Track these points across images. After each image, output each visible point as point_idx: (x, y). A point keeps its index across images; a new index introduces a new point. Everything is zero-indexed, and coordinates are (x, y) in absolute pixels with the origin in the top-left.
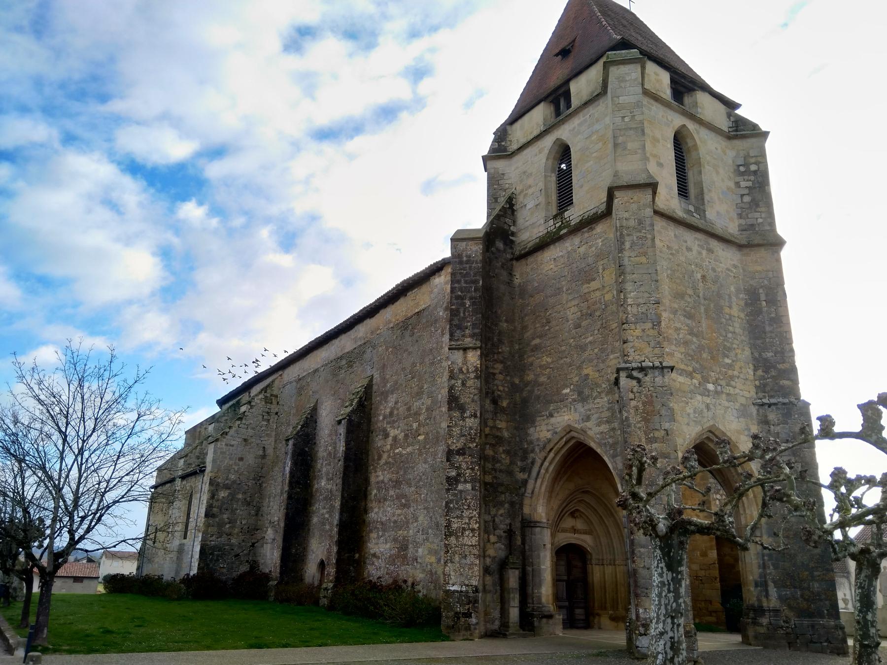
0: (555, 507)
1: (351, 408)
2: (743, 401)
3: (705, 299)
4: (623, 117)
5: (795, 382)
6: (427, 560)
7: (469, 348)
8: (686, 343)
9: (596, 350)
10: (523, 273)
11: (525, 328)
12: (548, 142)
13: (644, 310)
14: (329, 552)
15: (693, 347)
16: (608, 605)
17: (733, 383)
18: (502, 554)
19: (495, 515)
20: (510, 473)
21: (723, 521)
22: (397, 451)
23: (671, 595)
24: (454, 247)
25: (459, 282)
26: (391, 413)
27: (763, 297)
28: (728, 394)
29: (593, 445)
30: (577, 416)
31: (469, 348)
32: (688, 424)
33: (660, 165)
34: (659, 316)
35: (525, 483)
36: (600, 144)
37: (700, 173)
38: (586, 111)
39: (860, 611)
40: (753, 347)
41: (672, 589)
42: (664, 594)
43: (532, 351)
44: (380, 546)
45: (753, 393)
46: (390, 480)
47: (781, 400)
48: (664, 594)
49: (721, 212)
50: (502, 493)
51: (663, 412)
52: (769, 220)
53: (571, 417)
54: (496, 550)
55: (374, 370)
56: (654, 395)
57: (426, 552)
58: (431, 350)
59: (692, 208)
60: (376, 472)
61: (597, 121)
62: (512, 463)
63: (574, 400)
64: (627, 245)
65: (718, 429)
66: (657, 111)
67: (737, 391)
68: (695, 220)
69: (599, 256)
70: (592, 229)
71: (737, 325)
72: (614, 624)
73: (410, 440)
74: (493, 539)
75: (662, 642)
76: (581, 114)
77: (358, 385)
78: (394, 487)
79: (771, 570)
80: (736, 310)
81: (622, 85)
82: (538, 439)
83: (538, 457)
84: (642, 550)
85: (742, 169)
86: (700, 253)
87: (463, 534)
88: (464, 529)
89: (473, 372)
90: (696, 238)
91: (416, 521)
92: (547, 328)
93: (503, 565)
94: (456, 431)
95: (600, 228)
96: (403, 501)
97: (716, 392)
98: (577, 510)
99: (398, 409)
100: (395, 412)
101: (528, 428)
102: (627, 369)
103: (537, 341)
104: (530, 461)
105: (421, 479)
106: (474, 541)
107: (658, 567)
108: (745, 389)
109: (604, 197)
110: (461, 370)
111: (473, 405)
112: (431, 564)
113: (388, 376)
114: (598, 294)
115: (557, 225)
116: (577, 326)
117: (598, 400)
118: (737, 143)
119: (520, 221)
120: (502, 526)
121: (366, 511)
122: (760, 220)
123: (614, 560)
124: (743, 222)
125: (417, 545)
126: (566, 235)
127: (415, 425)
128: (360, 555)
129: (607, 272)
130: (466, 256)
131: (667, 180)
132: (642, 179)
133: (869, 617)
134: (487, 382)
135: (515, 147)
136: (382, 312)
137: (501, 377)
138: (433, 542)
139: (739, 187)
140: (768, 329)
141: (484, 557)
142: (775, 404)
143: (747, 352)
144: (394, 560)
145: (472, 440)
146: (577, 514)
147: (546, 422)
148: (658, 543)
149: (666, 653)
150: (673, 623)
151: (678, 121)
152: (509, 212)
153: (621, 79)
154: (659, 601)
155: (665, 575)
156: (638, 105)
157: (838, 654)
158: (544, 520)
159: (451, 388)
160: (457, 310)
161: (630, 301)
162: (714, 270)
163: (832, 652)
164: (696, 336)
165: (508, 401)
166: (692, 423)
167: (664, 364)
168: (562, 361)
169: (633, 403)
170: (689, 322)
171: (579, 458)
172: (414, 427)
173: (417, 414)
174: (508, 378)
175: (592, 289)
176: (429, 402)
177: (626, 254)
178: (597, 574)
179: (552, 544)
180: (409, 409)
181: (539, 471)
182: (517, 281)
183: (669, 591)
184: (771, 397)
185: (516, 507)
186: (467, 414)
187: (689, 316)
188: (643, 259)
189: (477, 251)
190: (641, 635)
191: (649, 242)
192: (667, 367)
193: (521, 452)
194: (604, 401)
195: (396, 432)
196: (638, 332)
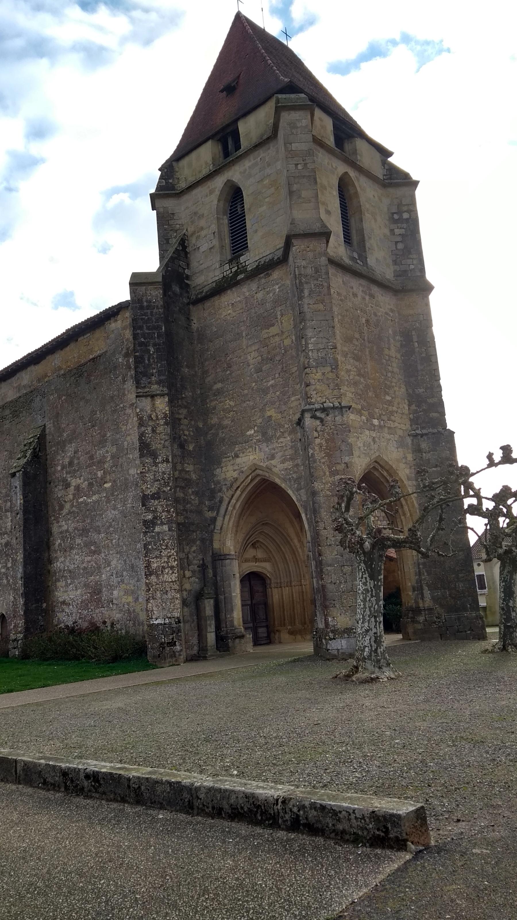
0: (240, 540)
1: (25, 460)
2: (400, 433)
3: (369, 342)
4: (297, 165)
5: (443, 414)
6: (124, 600)
7: (157, 395)
8: (356, 384)
9: (278, 393)
10: (200, 317)
11: (205, 373)
12: (219, 182)
13: (323, 355)
14: (15, 604)
15: (361, 387)
16: (287, 621)
17: (393, 418)
18: (197, 587)
19: (189, 552)
20: (200, 512)
21: (416, 535)
22: (81, 500)
23: (374, 598)
24: (133, 292)
25: (141, 328)
26: (71, 463)
27: (415, 338)
28: (389, 428)
29: (278, 481)
30: (262, 455)
31: (157, 395)
32: (359, 457)
33: (328, 212)
34: (336, 360)
35: (214, 520)
36: (273, 190)
37: (361, 220)
38: (256, 153)
39: (504, 600)
41: (374, 594)
42: (368, 599)
43: (215, 395)
45: (408, 426)
46: (76, 528)
47: (431, 430)
48: (368, 599)
49: (379, 259)
50: (193, 531)
51: (343, 448)
52: (419, 266)
53: (255, 457)
54: (192, 584)
55: (46, 419)
56: (335, 432)
57: (122, 593)
58: (112, 398)
59: (356, 255)
60: (58, 522)
61: (269, 165)
62: (201, 503)
63: (259, 441)
64: (306, 293)
65: (382, 459)
66: (323, 159)
67: (396, 424)
68: (359, 267)
69: (277, 302)
70: (269, 275)
71: (395, 365)
72: (292, 637)
74: (188, 574)
75: (368, 638)
76: (251, 157)
77: (28, 435)
78: (81, 535)
79: (425, 576)
80: (393, 352)
81: (294, 131)
82: (225, 479)
84: (329, 568)
85: (396, 217)
86: (364, 299)
87: (162, 572)
88: (163, 567)
89: (162, 419)
90: (360, 284)
91: (109, 565)
92: (228, 372)
93: (199, 597)
94: (150, 476)
95: (276, 274)
96: (92, 548)
97: (380, 427)
98: (258, 541)
99: (78, 458)
100: (76, 462)
102: (311, 410)
103: (219, 385)
105: (110, 526)
106: (174, 577)
107: (362, 577)
108: (402, 424)
109: (280, 243)
112: (128, 604)
113: (63, 426)
114: (277, 339)
115: (234, 270)
116: (259, 370)
117: (282, 440)
118: (391, 190)
119: (194, 264)
120: (195, 562)
121: (50, 562)
122: (412, 267)
123: (291, 582)
124: (397, 268)
125: (111, 588)
126: (242, 280)
127: (100, 474)
128: (48, 604)
129: (285, 318)
130: (147, 301)
131: (335, 225)
132: (316, 228)
133: (511, 604)
134: (173, 428)
135: (183, 185)
136: (50, 358)
137: (186, 422)
138: (129, 583)
139: (394, 234)
140: (420, 367)
142: (426, 434)
143: (403, 390)
144: (87, 605)
145: (166, 484)
146: (258, 545)
148: (363, 558)
149: (371, 646)
150: (376, 621)
151: (342, 168)
152: (183, 254)
153: (293, 125)
154: (364, 605)
155: (368, 584)
156: (310, 153)
157: (479, 639)
158: (233, 553)
159: (142, 435)
160: (142, 357)
161: (311, 347)
162: (375, 315)
163: (474, 638)
164: (363, 376)
165: (193, 445)
166: (362, 456)
167: (343, 404)
168: (245, 405)
169: (318, 441)
170: (357, 364)
171: (264, 492)
172: (99, 475)
173: (102, 462)
174: (193, 423)
175: (271, 334)
177: (306, 301)
178: (276, 596)
179: (239, 573)
180: (91, 458)
181: (227, 508)
182: (195, 325)
183: (372, 596)
184: (423, 428)
185: (207, 542)
186: (160, 459)
187: (357, 358)
188: (321, 307)
189: (157, 296)
190: (331, 639)
191: (325, 290)
192: (345, 407)
193: (211, 494)
194: (286, 440)
195: (79, 481)
196: (319, 376)
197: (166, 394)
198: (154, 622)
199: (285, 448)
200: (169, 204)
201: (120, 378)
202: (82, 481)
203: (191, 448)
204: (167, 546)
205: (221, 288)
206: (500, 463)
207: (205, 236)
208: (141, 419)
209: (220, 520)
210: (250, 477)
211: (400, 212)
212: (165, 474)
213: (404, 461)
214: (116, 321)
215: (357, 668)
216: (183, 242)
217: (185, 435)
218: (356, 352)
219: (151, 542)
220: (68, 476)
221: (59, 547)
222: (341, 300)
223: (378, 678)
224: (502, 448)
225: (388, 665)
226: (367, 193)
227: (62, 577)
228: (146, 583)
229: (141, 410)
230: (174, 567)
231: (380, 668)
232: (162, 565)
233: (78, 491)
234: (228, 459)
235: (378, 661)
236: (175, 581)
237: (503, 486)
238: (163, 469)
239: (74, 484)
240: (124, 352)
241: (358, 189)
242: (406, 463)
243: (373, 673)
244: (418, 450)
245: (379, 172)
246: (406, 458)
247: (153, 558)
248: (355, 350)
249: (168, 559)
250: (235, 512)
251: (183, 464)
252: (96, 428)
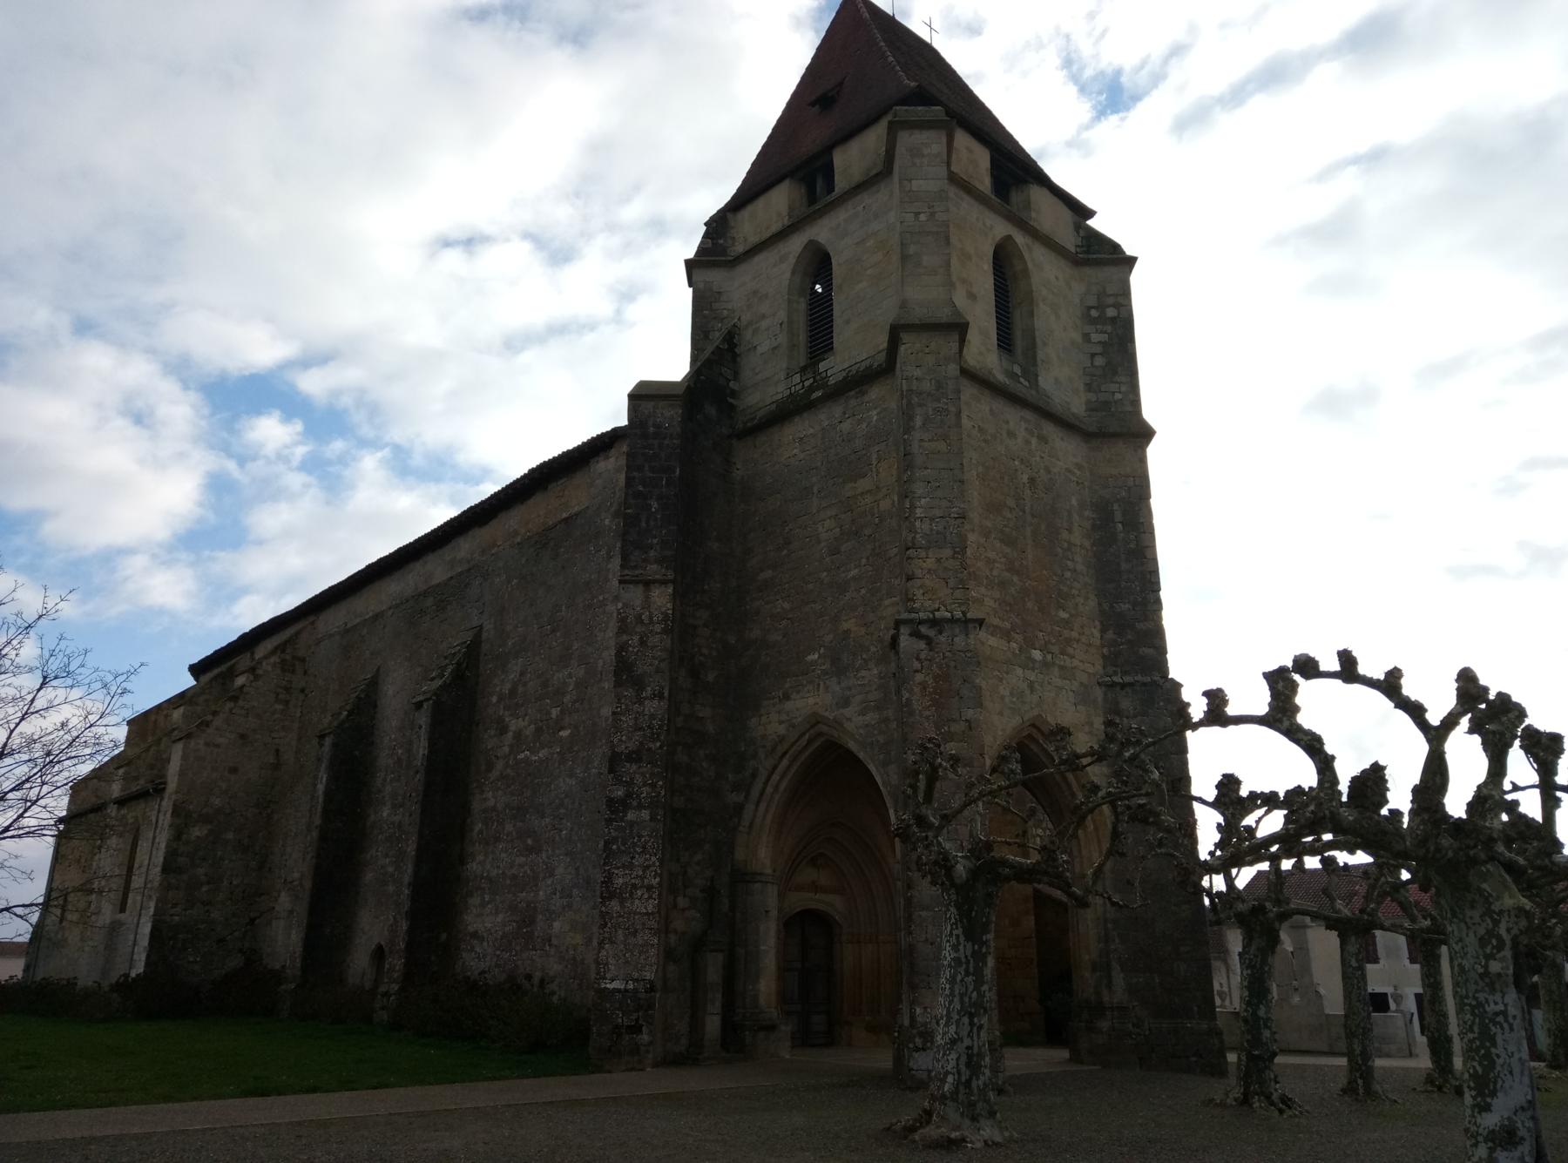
3: (1033, 516)
4: (917, 214)
5: (1162, 650)
8: (1003, 584)
12: (796, 244)
13: (940, 528)
21: (1055, 860)
22: (522, 756)
23: (970, 979)
26: (513, 692)
27: (1118, 516)
28: (1062, 668)
29: (852, 746)
31: (654, 582)
33: (972, 296)
35: (739, 809)
37: (1031, 314)
39: (1248, 1003)
42: (959, 978)
45: (1099, 668)
47: (1139, 678)
48: (959, 978)
49: (1062, 378)
59: (1017, 370)
63: (825, 673)
64: (918, 421)
66: (969, 210)
67: (1076, 662)
68: (1022, 388)
70: (864, 393)
71: (1078, 559)
74: (682, 902)
80: (1078, 536)
84: (924, 914)
85: (1094, 313)
86: (1028, 442)
87: (631, 894)
88: (634, 886)
91: (552, 875)
95: (875, 392)
96: (529, 841)
97: (1045, 664)
99: (525, 684)
100: (521, 689)
103: (768, 574)
108: (1087, 662)
109: (882, 341)
112: (575, 948)
115: (807, 384)
116: (834, 551)
117: (863, 673)
118: (1088, 271)
122: (1118, 396)
127: (555, 712)
132: (944, 315)
133: (1262, 1012)
135: (740, 248)
140: (1124, 566)
142: (1131, 685)
143: (1092, 603)
148: (954, 897)
149: (959, 1073)
150: (972, 1024)
151: (1001, 229)
159: (621, 648)
167: (969, 616)
169: (919, 677)
170: (1008, 550)
171: (830, 768)
176: (581, 672)
177: (917, 435)
183: (967, 973)
184: (1125, 673)
188: (942, 446)
190: (917, 1050)
194: (872, 673)
195: (521, 723)
200: (715, 277)
201: (603, 552)
203: (711, 677)
204: (644, 847)
205: (784, 413)
206: (1201, 723)
207: (767, 329)
208: (623, 620)
209: (750, 807)
211: (1101, 307)
213: (1087, 728)
215: (929, 1113)
216: (731, 338)
222: (986, 441)
223: (964, 1140)
224: (1207, 694)
225: (992, 1114)
226: (1046, 273)
229: (625, 605)
231: (974, 1119)
235: (972, 1105)
237: (1224, 776)
241: (1030, 265)
242: (1090, 733)
243: (958, 1128)
244: (1113, 710)
245: (1069, 241)
246: (1091, 724)
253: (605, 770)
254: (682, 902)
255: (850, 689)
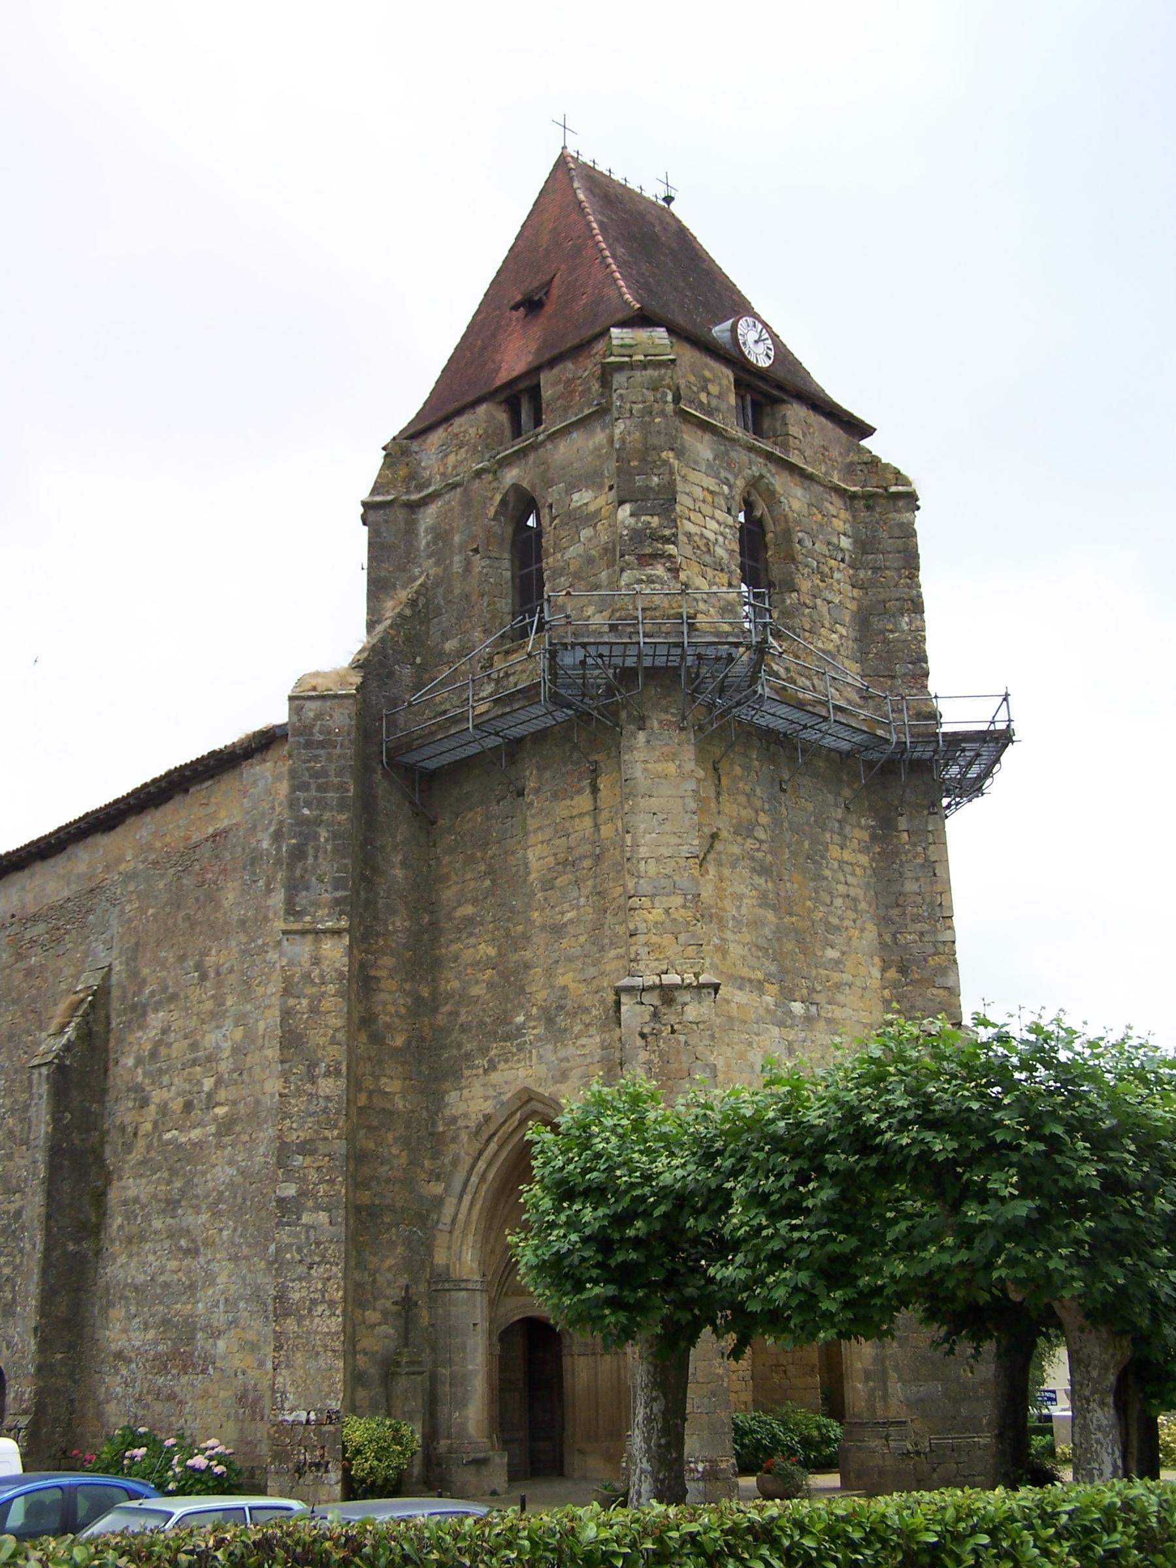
6: (237, 1363)
17: (840, 998)
22: (167, 1136)
25: (305, 787)
26: (154, 1054)
28: (829, 1021)
35: (438, 1203)
40: (884, 921)
44: (132, 1335)
46: (154, 1196)
55: (115, 952)
73: (197, 1113)
83: (465, 1147)
87: (310, 1310)
88: (314, 1302)
91: (213, 1283)
96: (183, 1242)
97: (808, 1020)
99: (169, 1045)
100: (163, 1051)
101: (448, 1092)
104: (447, 1160)
106: (335, 1323)
110: (307, 977)
111: (333, 1050)
127: (208, 1084)
141: (355, 1353)
143: (871, 932)
147: (482, 1080)
159: (287, 1013)
161: (643, 851)
170: (760, 881)
175: (575, 812)
176: (239, 1033)
193: (428, 1138)
194: (593, 1042)
195: (165, 1094)
196: (657, 914)
197: (345, 930)
198: (287, 1418)
199: (589, 1060)
202: (172, 1094)
210: (518, 1115)
212: (331, 1101)
214: (264, 761)
217: (386, 1015)
218: (760, 855)
219: (291, 1245)
220: (147, 1081)
221: (118, 1231)
227: (120, 1298)
228: (275, 1332)
230: (335, 1303)
232: (312, 1295)
233: (164, 1115)
234: (474, 1072)
236: (337, 1333)
238: (327, 1090)
239: (156, 1100)
240: (272, 829)
247: (294, 1281)
248: (758, 850)
249: (324, 1285)
250: (485, 1187)
251: (377, 1078)
252: (208, 984)
253: (272, 1160)
254: (372, 1316)
255: (567, 1059)
